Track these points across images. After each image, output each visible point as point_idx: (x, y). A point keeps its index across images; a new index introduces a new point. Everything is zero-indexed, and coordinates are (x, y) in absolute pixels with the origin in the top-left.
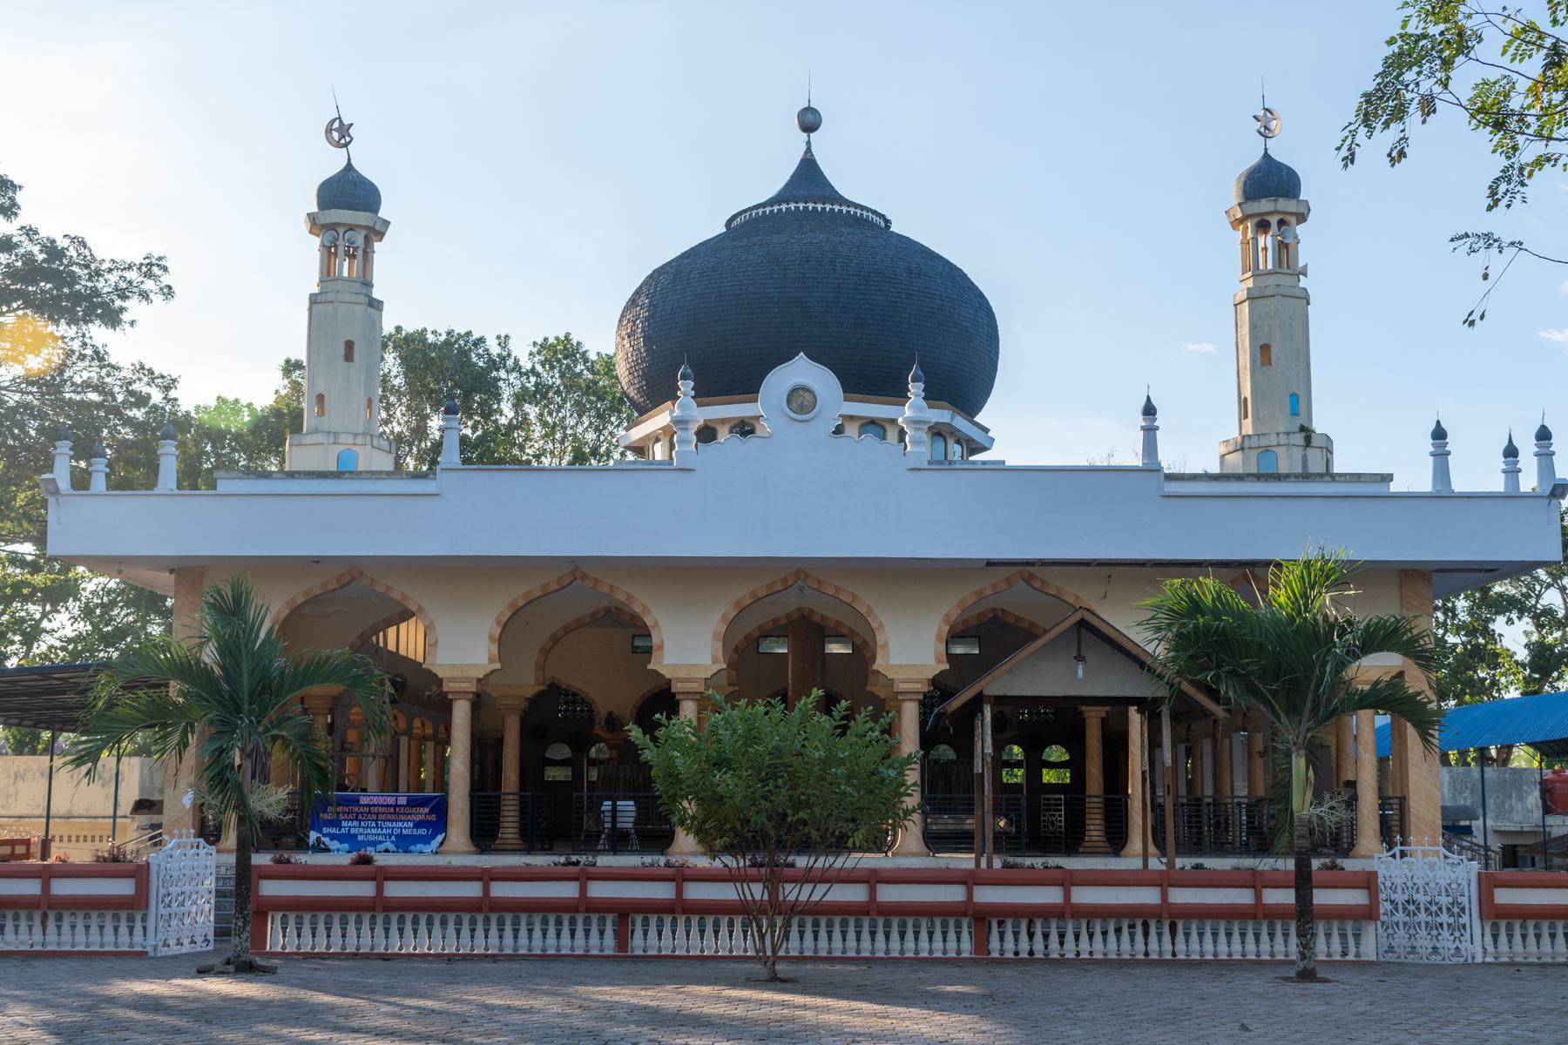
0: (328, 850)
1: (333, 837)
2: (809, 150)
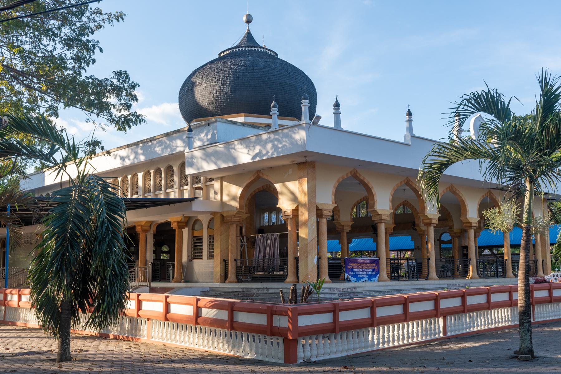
0: (350, 281)
1: (352, 276)
2: (249, 30)
